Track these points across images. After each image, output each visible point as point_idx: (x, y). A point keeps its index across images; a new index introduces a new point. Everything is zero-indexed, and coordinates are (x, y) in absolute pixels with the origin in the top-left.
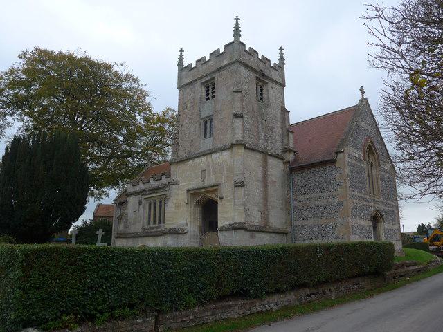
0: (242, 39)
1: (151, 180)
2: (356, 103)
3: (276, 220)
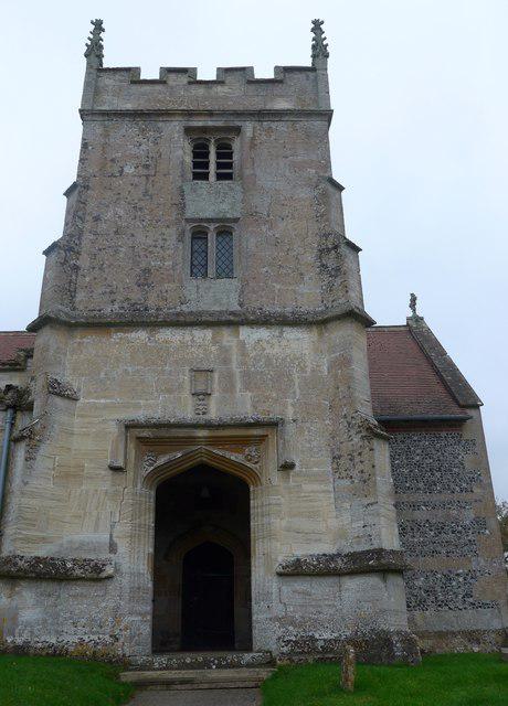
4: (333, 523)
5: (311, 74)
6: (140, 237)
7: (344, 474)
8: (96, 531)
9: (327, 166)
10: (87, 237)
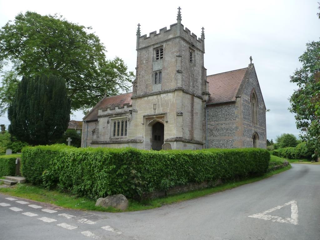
0: (182, 22)
1: (117, 108)
2: (247, 66)
3: (198, 136)
6: (146, 78)
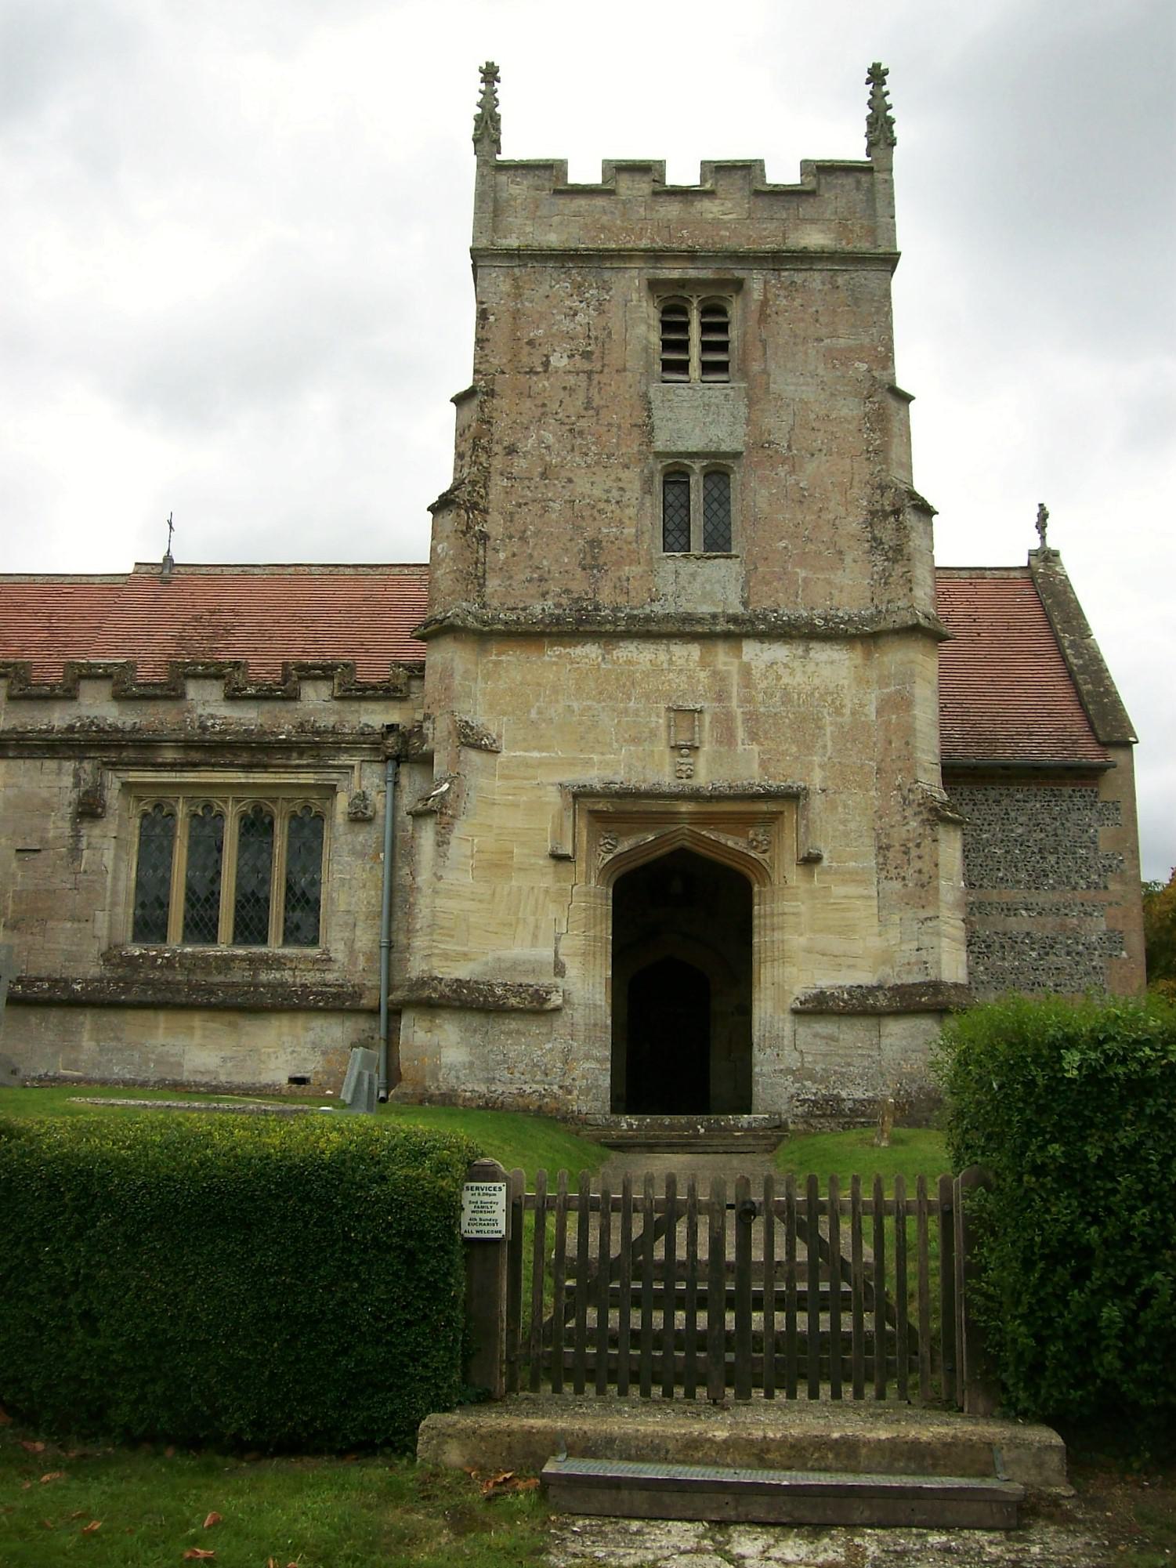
4: (875, 943)
5: (865, 179)
6: (582, 486)
7: (893, 873)
8: (533, 946)
9: (886, 359)
10: (498, 483)
